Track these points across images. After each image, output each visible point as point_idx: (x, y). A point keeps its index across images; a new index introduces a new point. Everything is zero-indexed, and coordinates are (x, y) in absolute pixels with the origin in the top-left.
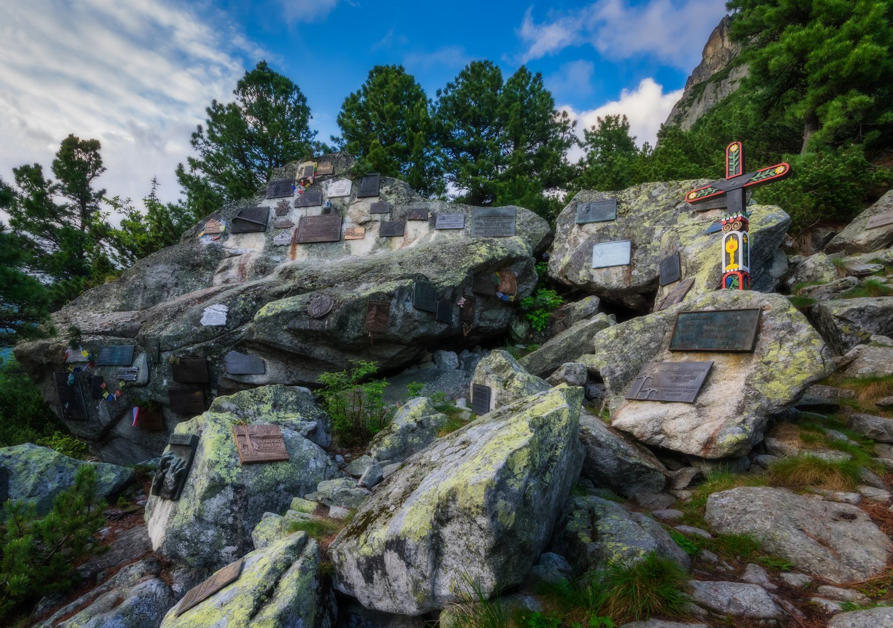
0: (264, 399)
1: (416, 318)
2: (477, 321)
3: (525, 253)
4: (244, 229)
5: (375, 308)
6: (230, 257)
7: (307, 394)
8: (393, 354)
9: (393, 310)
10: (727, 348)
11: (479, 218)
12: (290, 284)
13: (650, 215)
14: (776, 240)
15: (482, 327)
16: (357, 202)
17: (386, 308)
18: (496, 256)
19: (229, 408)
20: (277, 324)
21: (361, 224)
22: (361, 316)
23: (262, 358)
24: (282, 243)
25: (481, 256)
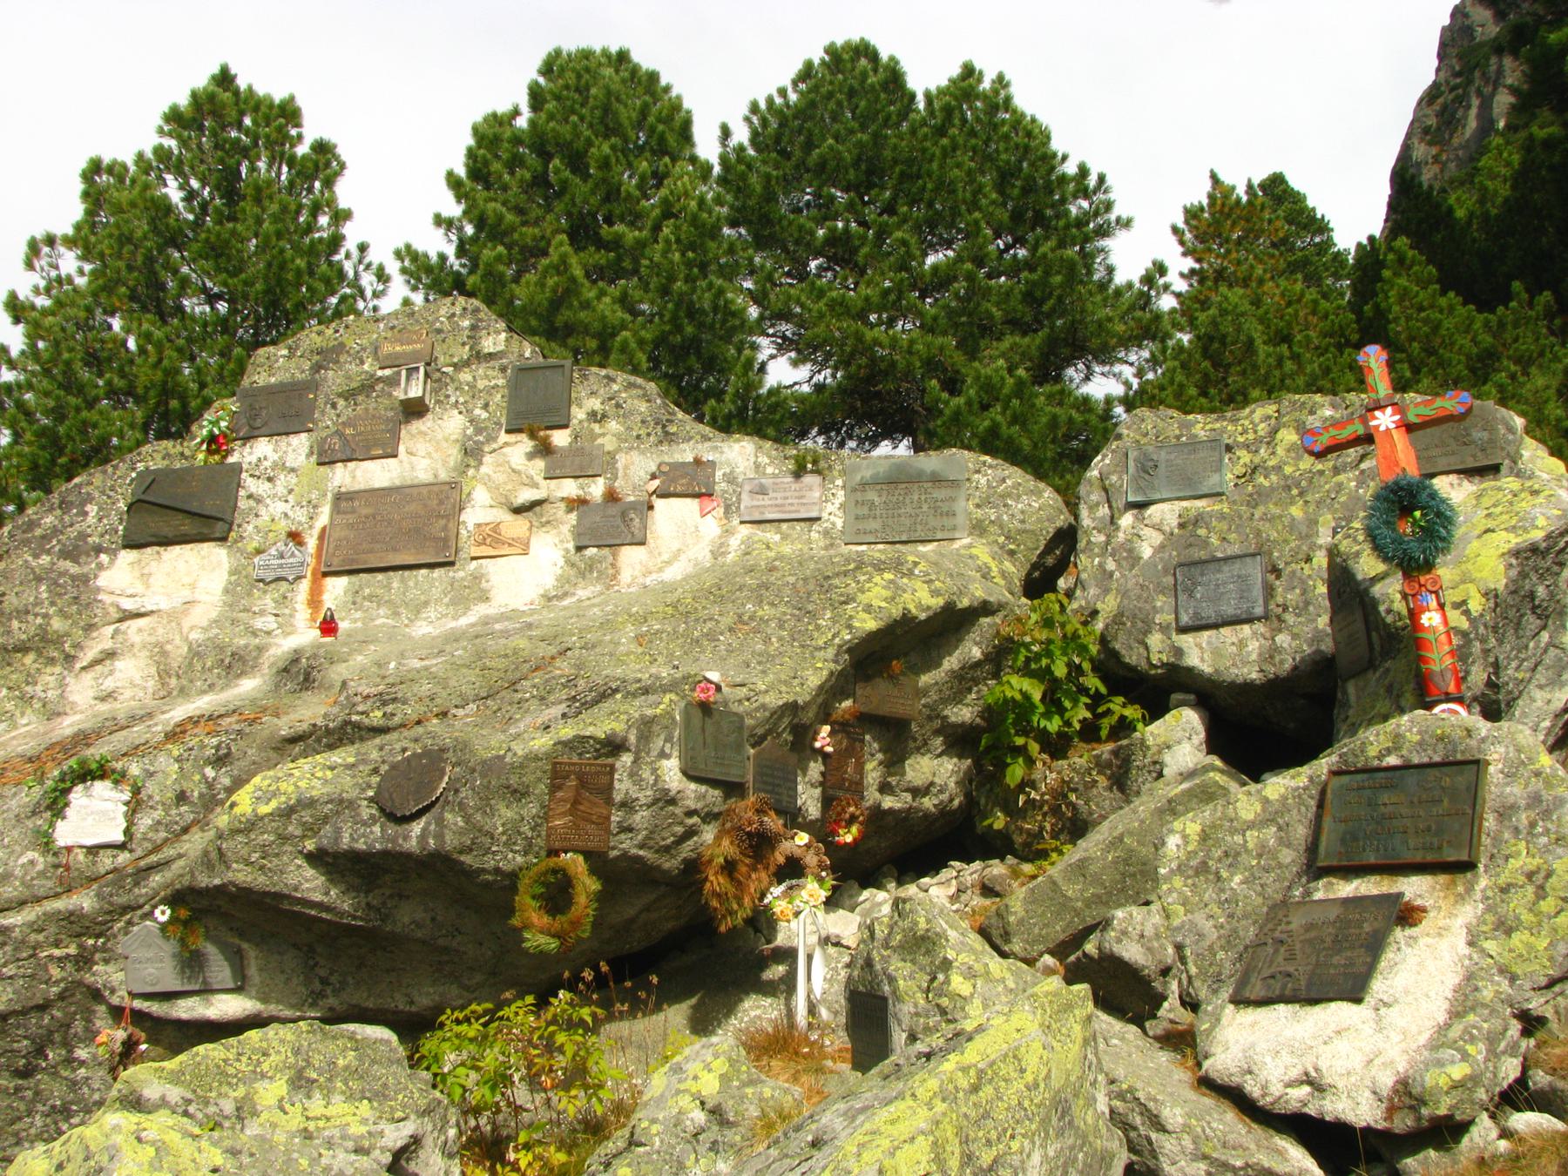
0: (265, 1067)
1: (691, 804)
2: (872, 796)
3: (998, 592)
4: (168, 531)
5: (572, 782)
6: (120, 620)
7: (388, 1042)
8: (631, 912)
9: (622, 786)
10: (1430, 858)
11: (864, 485)
12: (311, 711)
13: (1304, 483)
14: (1556, 568)
15: (891, 811)
16: (506, 444)
17: (604, 779)
18: (912, 607)
19: (163, 1098)
20: (284, 838)
21: (518, 511)
22: (532, 809)
23: (237, 941)
24: (280, 573)
25: (868, 609)
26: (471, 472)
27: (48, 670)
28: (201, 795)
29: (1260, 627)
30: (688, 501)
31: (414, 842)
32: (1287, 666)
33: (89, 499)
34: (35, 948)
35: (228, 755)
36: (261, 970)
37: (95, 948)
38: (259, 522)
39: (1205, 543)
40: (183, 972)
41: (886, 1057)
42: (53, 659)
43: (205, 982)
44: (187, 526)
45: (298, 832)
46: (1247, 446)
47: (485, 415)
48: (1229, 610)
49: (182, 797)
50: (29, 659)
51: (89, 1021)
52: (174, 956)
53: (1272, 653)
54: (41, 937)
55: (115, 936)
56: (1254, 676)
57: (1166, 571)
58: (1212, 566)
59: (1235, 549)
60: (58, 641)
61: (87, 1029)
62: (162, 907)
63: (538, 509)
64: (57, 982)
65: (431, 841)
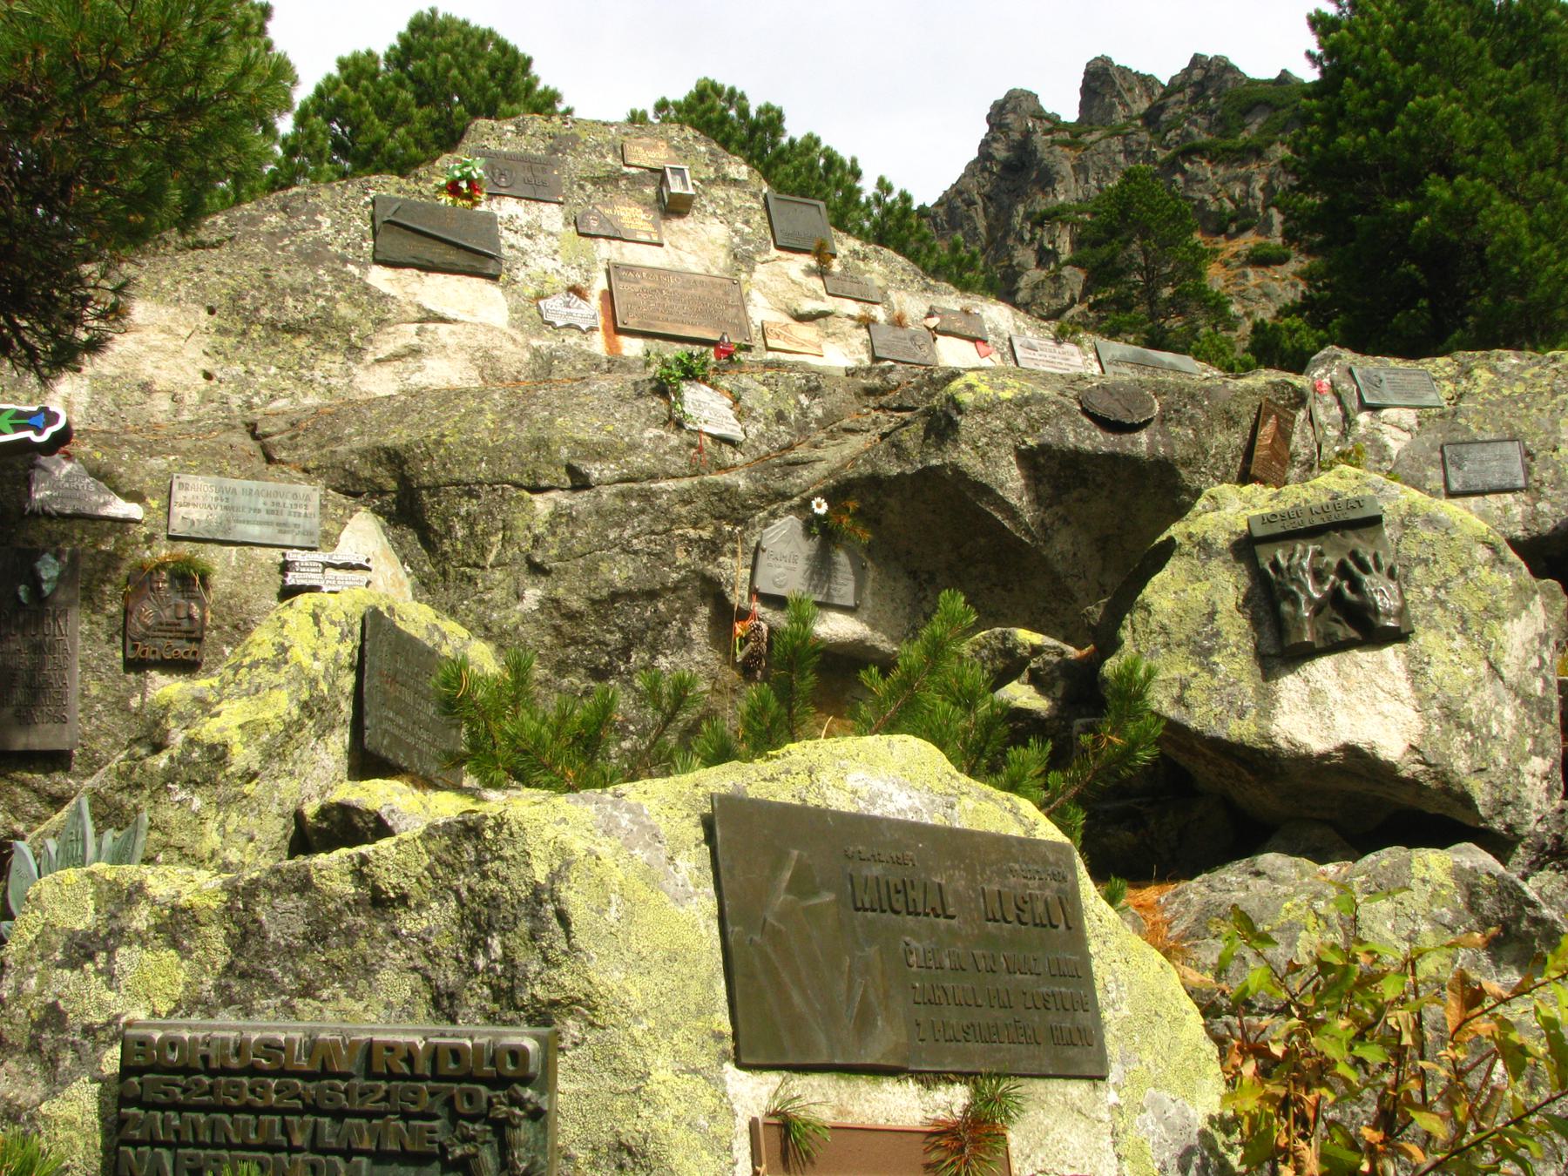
21: (801, 318)
26: (743, 276)
27: (327, 357)
28: (797, 420)
29: (1522, 496)
30: (965, 343)
31: (1144, 447)
32: (1550, 526)
33: (318, 210)
34: (673, 522)
35: (818, 388)
36: (874, 594)
37: (731, 537)
38: (530, 271)
39: (1467, 429)
40: (811, 579)
41: (1098, 875)
42: (333, 347)
43: (828, 595)
44: (452, 256)
45: (1022, 427)
46: (1449, 378)
47: (747, 230)
48: (1495, 481)
49: (780, 417)
50: (301, 343)
51: (686, 624)
52: (808, 559)
53: (1535, 516)
54: (684, 511)
55: (754, 526)
56: (1519, 533)
57: (1433, 449)
58: (1477, 446)
59: (1493, 436)
60: (344, 328)
61: (681, 633)
62: (818, 500)
63: (822, 321)
64: (680, 568)
65: (1161, 449)
